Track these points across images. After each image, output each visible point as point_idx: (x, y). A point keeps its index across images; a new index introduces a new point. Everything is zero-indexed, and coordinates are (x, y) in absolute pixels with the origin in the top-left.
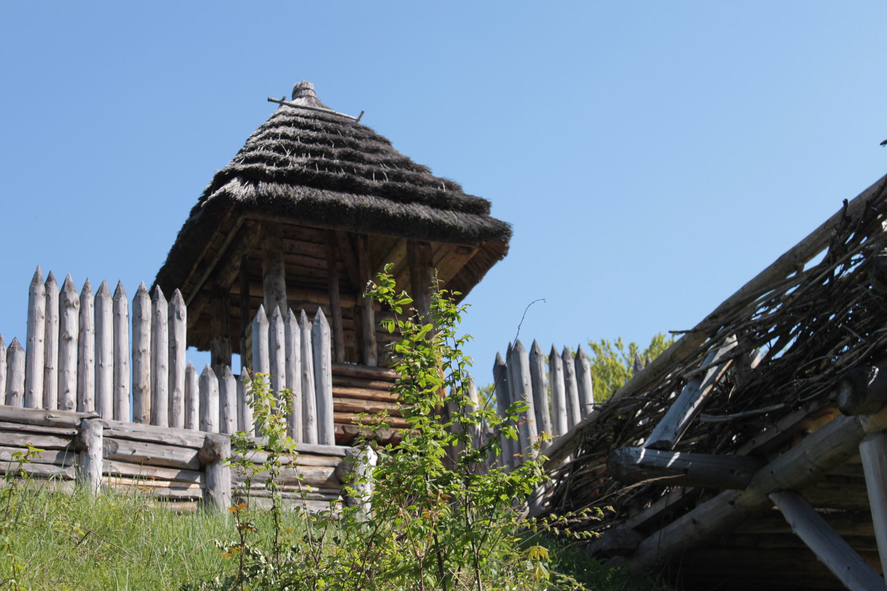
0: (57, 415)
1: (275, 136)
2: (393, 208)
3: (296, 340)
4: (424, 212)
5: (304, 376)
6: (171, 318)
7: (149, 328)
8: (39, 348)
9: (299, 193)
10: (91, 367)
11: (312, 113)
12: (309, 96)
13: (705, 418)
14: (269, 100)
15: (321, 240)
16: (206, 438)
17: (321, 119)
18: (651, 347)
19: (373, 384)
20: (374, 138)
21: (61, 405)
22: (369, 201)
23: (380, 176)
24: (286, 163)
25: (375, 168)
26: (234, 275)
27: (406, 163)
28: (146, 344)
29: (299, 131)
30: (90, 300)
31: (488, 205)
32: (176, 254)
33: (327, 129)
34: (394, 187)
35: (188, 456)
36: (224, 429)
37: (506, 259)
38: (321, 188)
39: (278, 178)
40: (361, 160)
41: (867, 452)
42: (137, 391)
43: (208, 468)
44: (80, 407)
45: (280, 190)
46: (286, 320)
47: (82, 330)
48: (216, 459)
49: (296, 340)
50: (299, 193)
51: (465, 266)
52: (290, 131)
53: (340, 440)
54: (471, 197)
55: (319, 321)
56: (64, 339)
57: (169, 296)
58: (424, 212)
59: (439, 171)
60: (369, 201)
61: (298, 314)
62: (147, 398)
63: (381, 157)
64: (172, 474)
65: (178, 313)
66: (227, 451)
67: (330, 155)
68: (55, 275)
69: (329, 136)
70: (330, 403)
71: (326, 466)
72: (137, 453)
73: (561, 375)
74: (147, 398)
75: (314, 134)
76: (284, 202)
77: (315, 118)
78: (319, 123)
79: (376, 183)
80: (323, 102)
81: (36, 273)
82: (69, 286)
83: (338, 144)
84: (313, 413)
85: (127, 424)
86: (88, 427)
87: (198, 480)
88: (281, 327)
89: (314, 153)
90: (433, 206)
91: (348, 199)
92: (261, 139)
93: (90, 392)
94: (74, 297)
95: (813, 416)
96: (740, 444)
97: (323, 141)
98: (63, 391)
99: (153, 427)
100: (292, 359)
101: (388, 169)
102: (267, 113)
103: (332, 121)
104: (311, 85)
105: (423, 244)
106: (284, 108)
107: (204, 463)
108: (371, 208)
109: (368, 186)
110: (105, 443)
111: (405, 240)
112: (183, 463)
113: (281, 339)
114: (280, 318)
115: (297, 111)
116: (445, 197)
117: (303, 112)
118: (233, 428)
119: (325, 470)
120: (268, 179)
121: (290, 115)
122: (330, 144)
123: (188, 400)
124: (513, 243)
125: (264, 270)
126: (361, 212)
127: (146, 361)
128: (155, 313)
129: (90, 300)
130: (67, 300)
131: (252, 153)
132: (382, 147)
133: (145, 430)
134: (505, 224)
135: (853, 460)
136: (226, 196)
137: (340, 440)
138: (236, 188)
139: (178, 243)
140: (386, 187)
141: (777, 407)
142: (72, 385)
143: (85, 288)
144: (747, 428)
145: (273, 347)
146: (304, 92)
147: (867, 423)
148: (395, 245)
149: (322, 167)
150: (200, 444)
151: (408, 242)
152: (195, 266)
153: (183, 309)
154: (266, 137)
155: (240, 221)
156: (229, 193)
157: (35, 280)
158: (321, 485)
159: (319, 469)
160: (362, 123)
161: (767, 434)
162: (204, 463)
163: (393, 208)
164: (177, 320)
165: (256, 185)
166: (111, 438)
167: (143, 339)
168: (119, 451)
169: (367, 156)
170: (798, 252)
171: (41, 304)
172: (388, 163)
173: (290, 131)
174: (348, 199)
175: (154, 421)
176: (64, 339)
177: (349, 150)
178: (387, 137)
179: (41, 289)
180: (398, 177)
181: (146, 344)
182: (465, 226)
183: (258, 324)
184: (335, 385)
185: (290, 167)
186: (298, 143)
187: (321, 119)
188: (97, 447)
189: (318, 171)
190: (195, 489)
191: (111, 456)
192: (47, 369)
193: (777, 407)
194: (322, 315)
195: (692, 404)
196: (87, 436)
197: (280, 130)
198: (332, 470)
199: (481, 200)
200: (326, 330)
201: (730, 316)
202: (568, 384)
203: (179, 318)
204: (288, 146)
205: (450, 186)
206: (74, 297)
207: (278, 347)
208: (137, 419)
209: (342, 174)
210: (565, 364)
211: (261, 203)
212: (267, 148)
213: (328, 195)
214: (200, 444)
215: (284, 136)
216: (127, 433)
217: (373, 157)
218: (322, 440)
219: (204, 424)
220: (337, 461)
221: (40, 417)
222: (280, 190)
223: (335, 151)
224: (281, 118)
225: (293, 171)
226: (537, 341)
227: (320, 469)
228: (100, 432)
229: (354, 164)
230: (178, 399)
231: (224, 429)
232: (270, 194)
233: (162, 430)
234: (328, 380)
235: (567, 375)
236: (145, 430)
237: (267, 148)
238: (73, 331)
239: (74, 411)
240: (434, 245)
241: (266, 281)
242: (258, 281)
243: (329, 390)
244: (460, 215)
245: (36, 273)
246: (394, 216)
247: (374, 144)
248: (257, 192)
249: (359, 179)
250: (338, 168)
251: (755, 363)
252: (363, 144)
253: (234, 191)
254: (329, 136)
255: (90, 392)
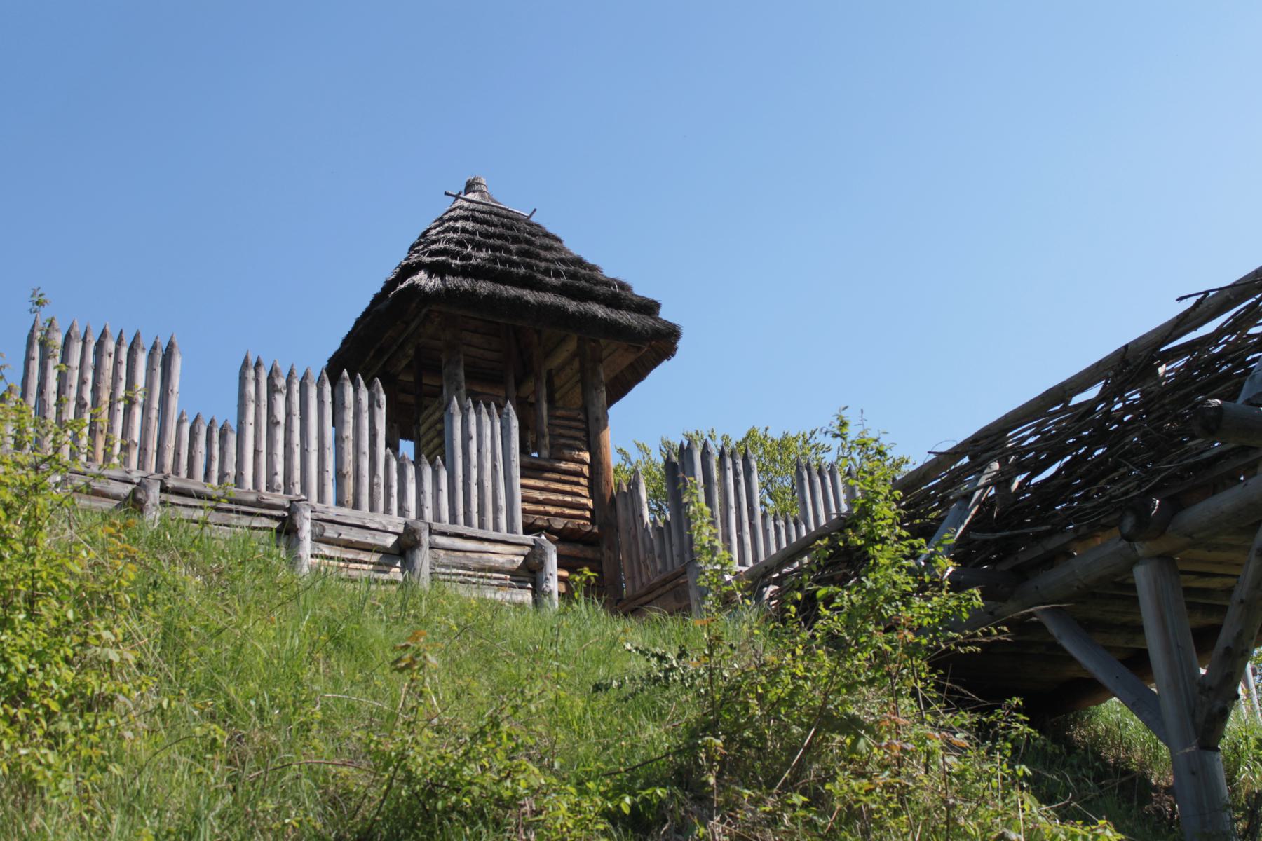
0: (268, 498)
1: (455, 230)
2: (572, 306)
3: (488, 431)
4: (600, 311)
5: (494, 467)
6: (371, 406)
7: (351, 414)
8: (250, 431)
9: (485, 287)
10: (297, 450)
11: (485, 208)
12: (481, 191)
13: (973, 536)
14: (446, 194)
15: (500, 333)
16: (406, 524)
17: (496, 214)
18: (745, 440)
19: (547, 475)
20: (547, 235)
21: (270, 487)
22: (549, 298)
23: (557, 274)
24: (469, 257)
25: (552, 266)
26: (404, 362)
27: (579, 262)
28: (349, 431)
29: (478, 226)
30: (296, 387)
31: (658, 306)
32: (351, 341)
33: (503, 225)
34: (572, 286)
35: (390, 541)
36: (420, 515)
37: (673, 359)
38: (504, 284)
39: (464, 272)
40: (538, 257)
41: (1142, 576)
42: (340, 476)
43: (408, 552)
44: (288, 490)
45: (466, 284)
46: (478, 413)
47: (289, 414)
48: (417, 544)
49: (488, 431)
50: (485, 287)
51: (631, 364)
52: (470, 225)
53: (528, 529)
54: (642, 298)
55: (508, 414)
56: (272, 423)
57: (369, 385)
58: (600, 311)
59: (611, 269)
60: (549, 298)
61: (488, 406)
62: (349, 483)
63: (554, 255)
64: (375, 558)
65: (379, 402)
66: (425, 538)
67: (508, 251)
68: (263, 360)
69: (507, 232)
70: (518, 493)
71: (517, 555)
72: (343, 537)
73: (730, 474)
74: (349, 483)
75: (492, 230)
76: (471, 295)
77: (491, 213)
78: (495, 219)
79: (552, 280)
80: (495, 197)
81: (246, 359)
82: (277, 371)
83: (516, 240)
84: (502, 502)
85: (332, 511)
86: (298, 509)
87: (399, 564)
88: (473, 418)
89: (495, 249)
90: (608, 306)
91: (530, 296)
92: (442, 232)
93: (297, 475)
94: (281, 383)
95: (1080, 538)
96: (999, 560)
97: (501, 237)
98: (271, 474)
99: (355, 512)
100: (483, 450)
101: (564, 268)
102: (443, 206)
103: (507, 217)
104: (483, 181)
105: (594, 341)
106: (459, 203)
107: (405, 548)
108: (552, 305)
109: (547, 284)
110: (313, 525)
111: (575, 337)
112: (385, 548)
113: (473, 430)
114: (472, 410)
115: (473, 206)
116: (618, 296)
117: (480, 207)
118: (428, 514)
119: (516, 558)
120: (455, 272)
121: (467, 209)
122: (507, 240)
123: (388, 487)
124: (681, 344)
125: (444, 361)
126: (541, 306)
127: (349, 447)
128: (357, 401)
129: (296, 387)
130: (275, 386)
131: (435, 246)
132: (556, 245)
133: (347, 514)
134: (675, 326)
135: (1130, 581)
136: (414, 288)
137: (528, 529)
138: (421, 278)
139: (354, 328)
140: (564, 284)
141: (1044, 528)
142: (280, 468)
143: (291, 374)
144: (1006, 549)
145: (466, 438)
146: (477, 187)
147: (1141, 549)
148: (563, 340)
149: (503, 263)
150: (401, 529)
151: (579, 339)
152: (372, 353)
153: (383, 397)
154: (447, 230)
155: (424, 311)
156: (418, 285)
157: (245, 364)
158: (513, 573)
159: (509, 557)
160: (534, 219)
161: (1025, 554)
162: (405, 548)
163: (572, 306)
164: (377, 409)
165: (442, 279)
166: (318, 521)
167: (346, 425)
168: (326, 534)
169: (543, 253)
170: (1067, 388)
171: (251, 388)
172: (563, 261)
173: (470, 225)
174: (530, 296)
175: (356, 506)
176: (272, 423)
177: (526, 247)
178: (559, 235)
179: (251, 373)
180: (573, 276)
181: (349, 431)
182: (639, 327)
183: (452, 415)
184: (522, 476)
185: (473, 262)
186: (478, 238)
187: (496, 214)
188: (306, 529)
189: (499, 267)
190: (396, 573)
191: (319, 539)
192: (256, 452)
193: (1044, 528)
194: (511, 408)
195: (962, 522)
196: (298, 518)
197: (459, 224)
198: (521, 559)
199: (653, 301)
200: (515, 423)
201: (986, 444)
202: (737, 483)
203: (379, 406)
204: (469, 241)
205: (623, 286)
206: (281, 383)
207: (471, 438)
208: (340, 502)
209: (522, 270)
210: (734, 464)
211: (449, 295)
212: (449, 241)
213: (512, 291)
214: (401, 529)
215: (464, 230)
216: (331, 516)
217: (548, 255)
218: (511, 529)
219: (402, 511)
220: (527, 550)
221: (252, 498)
222: (466, 284)
223: (513, 247)
224: (458, 212)
225: (478, 265)
226: (175, 340)
227: (511, 557)
228: (308, 514)
229: (533, 261)
230: (378, 484)
231: (420, 515)
232: (458, 288)
233: (363, 515)
234: (516, 471)
235: (736, 474)
236: (347, 514)
237: (449, 241)
238: (281, 415)
239: (281, 493)
240: (603, 342)
241: (445, 371)
242: (437, 371)
243: (517, 481)
244: (634, 315)
245: (246, 359)
246: (573, 314)
247: (548, 242)
248: (445, 285)
249: (540, 276)
250: (518, 265)
251: (1015, 486)
252: (538, 241)
253: (423, 283)
254: (507, 232)
255: (297, 475)
